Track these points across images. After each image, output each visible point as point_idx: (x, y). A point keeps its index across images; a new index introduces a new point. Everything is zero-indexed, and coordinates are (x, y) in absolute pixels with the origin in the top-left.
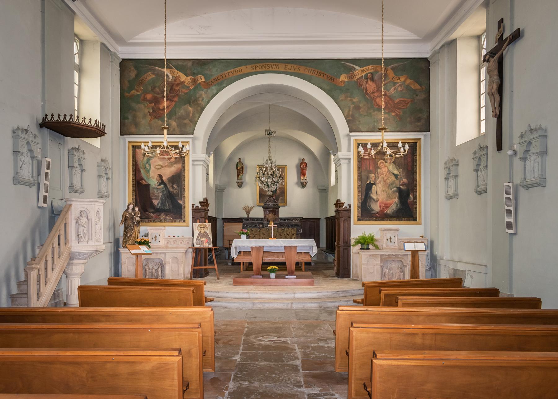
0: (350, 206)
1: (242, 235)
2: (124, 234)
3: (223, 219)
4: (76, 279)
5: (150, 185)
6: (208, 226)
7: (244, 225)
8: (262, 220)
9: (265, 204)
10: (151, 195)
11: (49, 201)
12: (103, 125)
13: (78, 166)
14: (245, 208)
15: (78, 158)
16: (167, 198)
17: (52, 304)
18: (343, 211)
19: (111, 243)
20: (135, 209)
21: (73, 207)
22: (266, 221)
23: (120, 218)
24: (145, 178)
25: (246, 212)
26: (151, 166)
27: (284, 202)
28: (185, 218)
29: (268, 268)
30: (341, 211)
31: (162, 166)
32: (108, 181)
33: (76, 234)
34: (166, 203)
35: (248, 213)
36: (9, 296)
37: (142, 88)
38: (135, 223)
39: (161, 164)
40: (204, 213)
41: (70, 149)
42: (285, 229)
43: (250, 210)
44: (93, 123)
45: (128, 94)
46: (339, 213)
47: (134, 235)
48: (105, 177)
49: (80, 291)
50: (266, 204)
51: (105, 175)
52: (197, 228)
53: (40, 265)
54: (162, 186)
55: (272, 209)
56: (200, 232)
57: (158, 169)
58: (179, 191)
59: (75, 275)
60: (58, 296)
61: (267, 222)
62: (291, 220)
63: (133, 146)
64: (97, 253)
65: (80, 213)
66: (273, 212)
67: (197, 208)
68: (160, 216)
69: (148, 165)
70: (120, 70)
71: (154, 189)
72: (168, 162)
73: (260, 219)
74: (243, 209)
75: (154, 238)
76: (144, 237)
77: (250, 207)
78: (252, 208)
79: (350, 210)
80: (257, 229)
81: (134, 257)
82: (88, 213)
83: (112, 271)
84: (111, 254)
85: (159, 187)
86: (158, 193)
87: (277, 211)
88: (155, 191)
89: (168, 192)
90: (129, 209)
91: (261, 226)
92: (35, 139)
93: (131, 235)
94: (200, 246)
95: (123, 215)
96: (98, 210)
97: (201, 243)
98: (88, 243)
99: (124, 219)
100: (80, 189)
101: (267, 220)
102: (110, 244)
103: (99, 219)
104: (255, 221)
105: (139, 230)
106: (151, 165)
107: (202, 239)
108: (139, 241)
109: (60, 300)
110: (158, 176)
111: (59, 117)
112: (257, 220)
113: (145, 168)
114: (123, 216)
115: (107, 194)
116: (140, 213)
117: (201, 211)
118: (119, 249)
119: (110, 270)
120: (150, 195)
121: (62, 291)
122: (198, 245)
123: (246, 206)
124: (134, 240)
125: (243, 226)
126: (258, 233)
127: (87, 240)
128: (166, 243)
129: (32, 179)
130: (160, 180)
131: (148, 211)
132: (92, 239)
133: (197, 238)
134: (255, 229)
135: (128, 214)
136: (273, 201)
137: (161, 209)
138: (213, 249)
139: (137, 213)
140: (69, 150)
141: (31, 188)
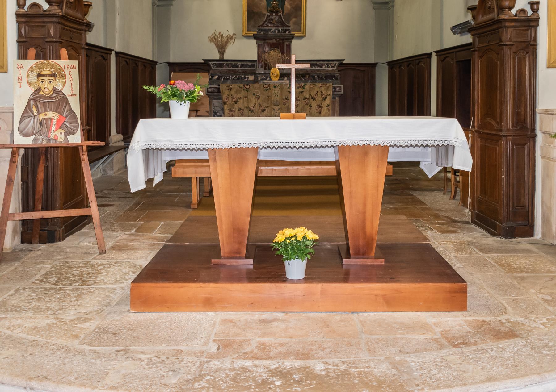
0: (535, 7)
1: (174, 104)
3: (170, 65)
6: (67, 71)
7: (213, 77)
8: (253, 66)
9: (260, 28)
14: (214, 37)
18: (513, 24)
22: (262, 67)
25: (217, 46)
27: (300, 27)
29: (276, 240)
30: (508, 24)
35: (222, 48)
40: (58, 26)
42: (307, 86)
43: (227, 42)
46: (498, 28)
50: (262, 28)
55: (276, 40)
56: (39, 90)
61: (265, 69)
62: (318, 65)
66: (278, 48)
67: (35, 10)
73: (249, 63)
74: (211, 40)
77: (225, 35)
78: (231, 38)
79: (537, 20)
80: (242, 85)
87: (287, 45)
91: (251, 78)
94: (35, 140)
97: (38, 128)
101: (265, 64)
104: (237, 67)
107: (42, 116)
112: (242, 65)
117: (46, 19)
122: (26, 135)
123: (217, 34)
125: (210, 79)
126: (243, 94)
133: (26, 111)
134: (236, 85)
136: (278, 22)
138: (85, 148)
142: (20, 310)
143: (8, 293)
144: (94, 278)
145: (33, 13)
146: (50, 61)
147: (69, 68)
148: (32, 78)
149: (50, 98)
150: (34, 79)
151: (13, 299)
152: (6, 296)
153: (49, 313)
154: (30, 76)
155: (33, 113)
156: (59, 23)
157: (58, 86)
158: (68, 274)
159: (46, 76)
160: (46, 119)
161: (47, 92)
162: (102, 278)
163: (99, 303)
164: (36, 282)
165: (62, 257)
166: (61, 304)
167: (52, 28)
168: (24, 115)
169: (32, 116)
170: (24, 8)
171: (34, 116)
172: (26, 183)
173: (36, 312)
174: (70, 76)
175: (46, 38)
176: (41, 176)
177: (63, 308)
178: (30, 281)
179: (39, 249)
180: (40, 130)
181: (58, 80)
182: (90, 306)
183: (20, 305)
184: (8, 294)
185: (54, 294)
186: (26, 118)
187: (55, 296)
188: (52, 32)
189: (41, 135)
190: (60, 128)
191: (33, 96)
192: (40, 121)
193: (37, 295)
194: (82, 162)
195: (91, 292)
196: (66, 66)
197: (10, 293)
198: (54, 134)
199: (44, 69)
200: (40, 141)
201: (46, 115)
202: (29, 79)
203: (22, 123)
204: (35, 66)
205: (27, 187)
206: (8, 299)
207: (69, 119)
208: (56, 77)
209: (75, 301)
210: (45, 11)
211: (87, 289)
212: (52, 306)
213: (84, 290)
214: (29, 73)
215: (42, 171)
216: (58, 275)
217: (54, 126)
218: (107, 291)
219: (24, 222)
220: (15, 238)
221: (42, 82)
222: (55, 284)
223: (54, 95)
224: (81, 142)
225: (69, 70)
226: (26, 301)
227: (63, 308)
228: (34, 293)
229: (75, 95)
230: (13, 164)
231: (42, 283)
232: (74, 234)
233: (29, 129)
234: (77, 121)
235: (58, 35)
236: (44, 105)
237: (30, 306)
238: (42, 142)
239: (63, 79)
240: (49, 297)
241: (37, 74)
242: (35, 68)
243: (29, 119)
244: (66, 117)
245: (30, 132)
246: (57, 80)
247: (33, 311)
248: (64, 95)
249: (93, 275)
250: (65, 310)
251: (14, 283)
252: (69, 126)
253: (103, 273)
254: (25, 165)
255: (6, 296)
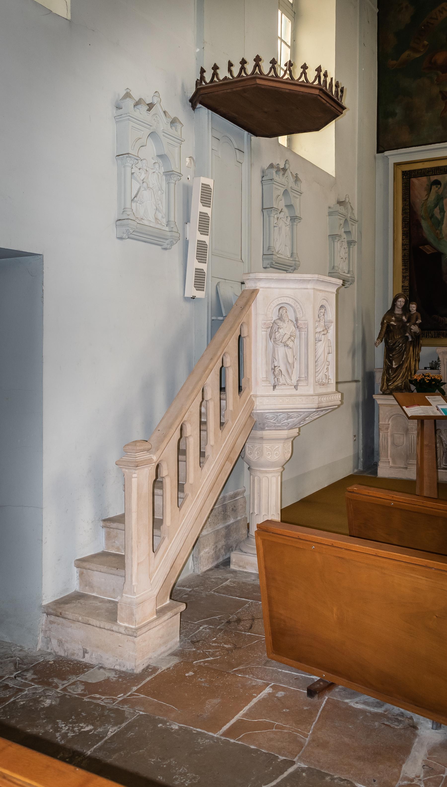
2: (385, 363)
4: (269, 475)
5: (443, 254)
11: (209, 284)
12: (337, 86)
13: (285, 210)
15: (282, 190)
17: (218, 531)
19: (356, 381)
20: (411, 309)
21: (260, 297)
23: (377, 329)
26: (444, 212)
32: (351, 249)
33: (267, 363)
36: (102, 524)
37: (426, 43)
38: (410, 339)
41: (266, 168)
44: (311, 75)
45: (394, 62)
47: (406, 365)
48: (346, 240)
49: (264, 541)
51: (344, 236)
53: (159, 452)
59: (268, 466)
60: (234, 510)
63: (404, 173)
64: (322, 413)
65: (279, 311)
70: (378, 13)
76: (428, 371)
81: (414, 424)
82: (297, 311)
83: (358, 442)
84: (356, 406)
90: (396, 308)
92: (173, 128)
93: (400, 366)
95: (384, 319)
96: (324, 303)
98: (297, 390)
99: (384, 330)
100: (287, 261)
102: (354, 385)
103: (326, 329)
105: (418, 354)
106: (445, 210)
108: (419, 378)
109: (239, 518)
111: (230, 71)
113: (431, 218)
114: (382, 324)
115: (349, 275)
116: (420, 317)
118: (374, 396)
119: (355, 440)
121: (244, 497)
124: (407, 377)
127: (294, 382)
129: (167, 229)
132: (307, 378)
135: (393, 318)
139: (415, 316)
140: (263, 172)
141: (166, 252)
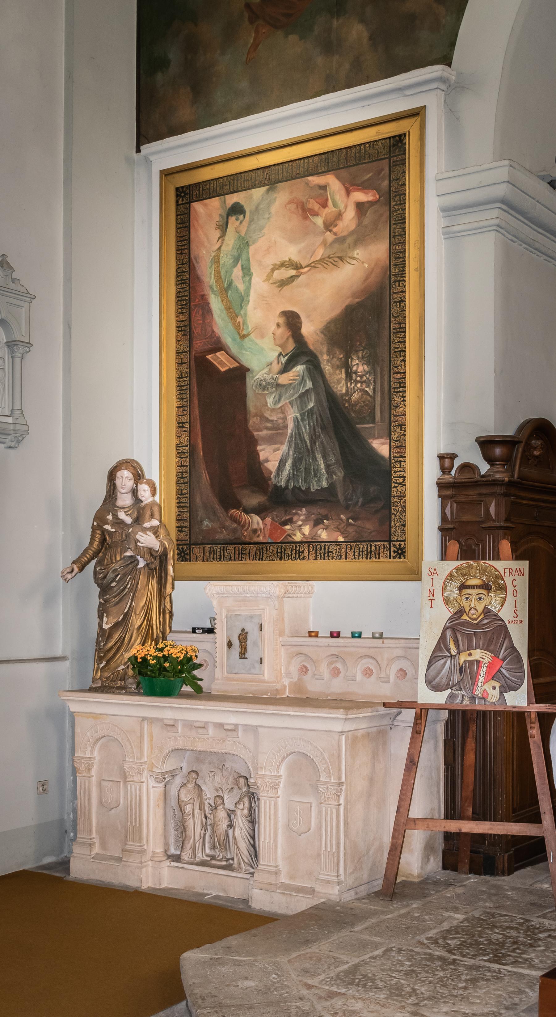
5: (248, 370)
6: (508, 580)
10: (253, 422)
16: (318, 430)
24: (228, 339)
26: (250, 275)
28: (404, 532)
31: (297, 267)
34: (315, 459)
39: (296, 258)
52: (444, 587)
54: (300, 369)
56: (460, 612)
57: (283, 283)
58: (374, 390)
67: (466, 477)
68: (288, 527)
69: (240, 273)
71: (264, 388)
72: (324, 243)
75: (236, 643)
85: (284, 379)
86: (282, 410)
88: (270, 401)
89: (325, 404)
94: (451, 697)
97: (456, 678)
106: (252, 270)
107: (463, 657)
110: (281, 320)
117: (484, 490)
120: (246, 421)
122: (437, 688)
128: (294, 668)
130: (291, 341)
131: (237, 504)
133: (438, 648)
137: (295, 487)
138: (534, 716)
142: (371, 985)
143: (372, 952)
144: (519, 953)
145: (463, 480)
146: (482, 562)
147: (513, 573)
148: (451, 591)
149: (478, 625)
150: (454, 593)
151: (373, 964)
152: (366, 957)
153: (410, 1001)
154: (448, 588)
155: (449, 652)
156: (506, 495)
157: (492, 605)
158: (483, 937)
159: (474, 588)
160: (471, 663)
161: (474, 616)
162: (533, 955)
163: (498, 1001)
164: (426, 941)
165: (491, 905)
166: (438, 989)
167: (493, 503)
168: (435, 655)
169: (448, 656)
170: (451, 473)
171: (451, 656)
172: (451, 768)
173: (391, 994)
174: (514, 588)
175: (483, 522)
176: (470, 758)
177: (435, 998)
178: (417, 938)
179: (465, 883)
180: (459, 680)
181: (493, 595)
182: (479, 1003)
183: (376, 978)
184: (370, 955)
185: (438, 968)
186: (438, 658)
187: (437, 973)
188: (492, 510)
189: (461, 690)
190: (493, 678)
191: (451, 622)
192: (461, 664)
193: (410, 966)
194: (531, 741)
195: (498, 977)
196: (507, 571)
197: (376, 953)
198: (483, 689)
199: (470, 576)
200: (459, 699)
201: (470, 655)
202: (446, 594)
203: (432, 668)
204: (456, 571)
205: (453, 775)
206: (366, 964)
207: (508, 664)
208: (491, 589)
209: (461, 988)
210: (483, 476)
211: (494, 972)
212: (423, 989)
213: (490, 971)
214: (447, 584)
215: (472, 750)
216: (465, 937)
217: (482, 675)
218: (525, 981)
219: (448, 836)
220: (428, 859)
221: (467, 598)
222: (450, 952)
223: (486, 621)
224: (528, 705)
225: (512, 578)
226: (389, 973)
227: (435, 998)
228: (409, 960)
229: (521, 622)
230: (416, 735)
231: (432, 946)
232: (537, 866)
233: (442, 678)
234: (522, 667)
235: (503, 516)
236: (469, 638)
237: (388, 983)
238: (462, 701)
239: (502, 593)
240: (427, 972)
241: (458, 584)
242: (456, 575)
243: (442, 661)
244: (504, 660)
245: (443, 683)
246: (492, 594)
247: (388, 992)
248: (502, 620)
249: (521, 947)
250: (436, 1002)
251: (391, 936)
252: (508, 676)
253: (539, 946)
254: (450, 738)
255: (366, 957)
